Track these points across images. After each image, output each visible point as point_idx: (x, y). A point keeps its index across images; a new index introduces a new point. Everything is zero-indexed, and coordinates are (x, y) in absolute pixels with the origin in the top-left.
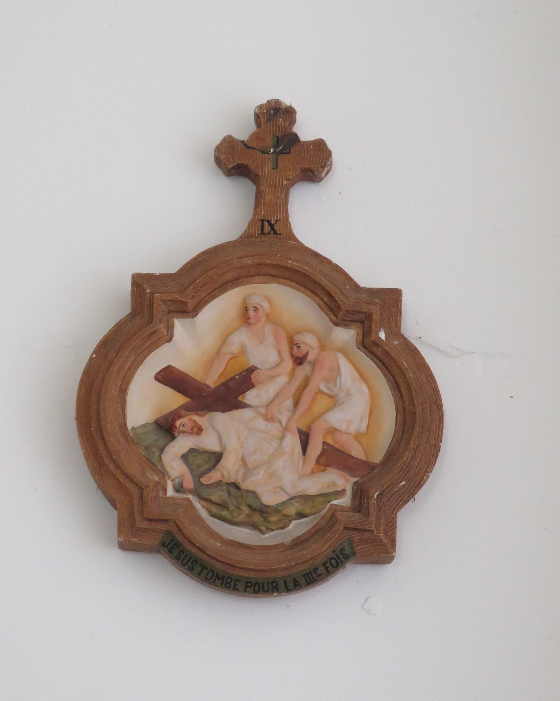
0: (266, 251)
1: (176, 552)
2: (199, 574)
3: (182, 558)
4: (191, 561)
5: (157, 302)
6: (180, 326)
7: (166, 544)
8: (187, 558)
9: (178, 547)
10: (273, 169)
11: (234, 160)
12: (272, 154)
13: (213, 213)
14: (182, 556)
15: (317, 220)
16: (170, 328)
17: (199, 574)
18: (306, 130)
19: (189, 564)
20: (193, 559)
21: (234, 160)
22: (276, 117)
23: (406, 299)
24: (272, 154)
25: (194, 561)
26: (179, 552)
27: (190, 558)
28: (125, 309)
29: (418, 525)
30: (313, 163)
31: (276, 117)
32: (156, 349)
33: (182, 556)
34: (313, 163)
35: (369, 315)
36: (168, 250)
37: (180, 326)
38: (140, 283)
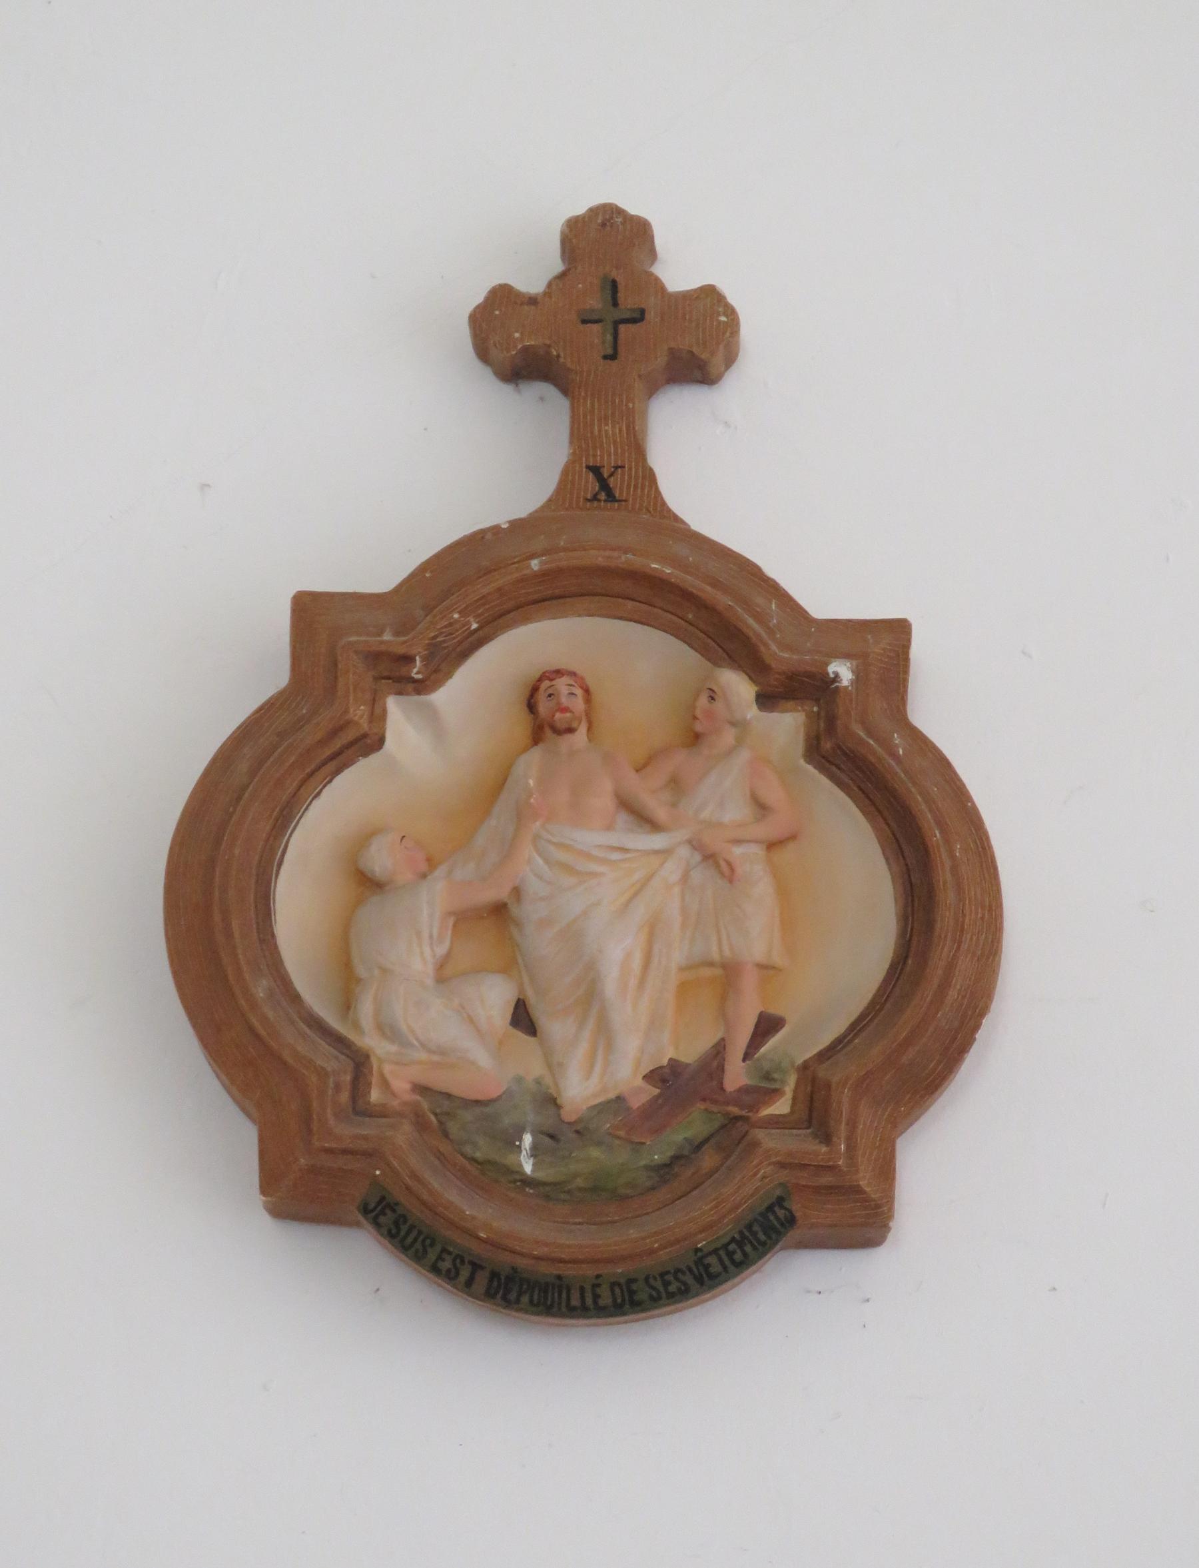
0: (607, 547)
1: (387, 1219)
2: (469, 1283)
3: (403, 1233)
4: (422, 1237)
5: (350, 663)
6: (400, 719)
7: (372, 1206)
8: (414, 1233)
9: (394, 1211)
10: (605, 357)
11: (515, 341)
12: (602, 328)
13: (483, 463)
14: (404, 1229)
15: (711, 467)
16: (379, 717)
17: (469, 1283)
18: (678, 270)
19: (418, 1245)
20: (555, 1310)
21: (515, 341)
22: (607, 245)
23: (920, 649)
24: (602, 328)
25: (427, 1237)
26: (454, 1260)
27: (582, 1289)
28: (279, 677)
29: (941, 1162)
30: (697, 343)
31: (607, 245)
32: (194, 1026)
33: (404, 1229)
34: (697, 343)
35: (847, 711)
36: (375, 562)
37: (400, 719)
38: (310, 611)
